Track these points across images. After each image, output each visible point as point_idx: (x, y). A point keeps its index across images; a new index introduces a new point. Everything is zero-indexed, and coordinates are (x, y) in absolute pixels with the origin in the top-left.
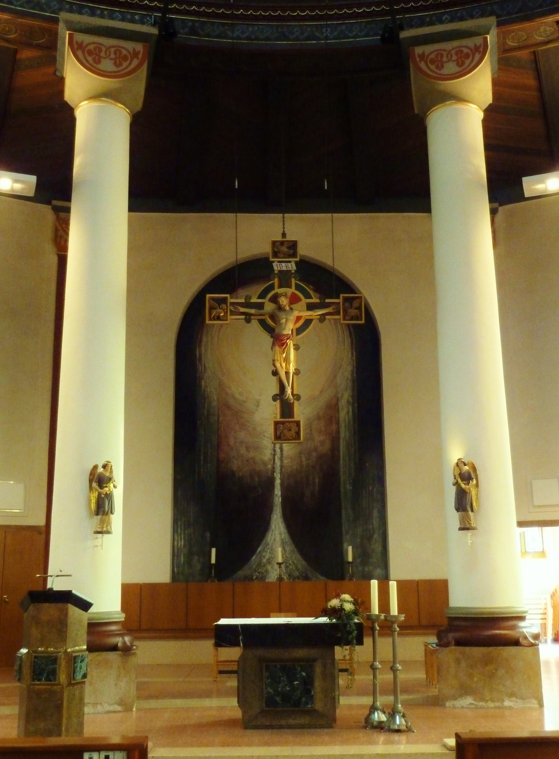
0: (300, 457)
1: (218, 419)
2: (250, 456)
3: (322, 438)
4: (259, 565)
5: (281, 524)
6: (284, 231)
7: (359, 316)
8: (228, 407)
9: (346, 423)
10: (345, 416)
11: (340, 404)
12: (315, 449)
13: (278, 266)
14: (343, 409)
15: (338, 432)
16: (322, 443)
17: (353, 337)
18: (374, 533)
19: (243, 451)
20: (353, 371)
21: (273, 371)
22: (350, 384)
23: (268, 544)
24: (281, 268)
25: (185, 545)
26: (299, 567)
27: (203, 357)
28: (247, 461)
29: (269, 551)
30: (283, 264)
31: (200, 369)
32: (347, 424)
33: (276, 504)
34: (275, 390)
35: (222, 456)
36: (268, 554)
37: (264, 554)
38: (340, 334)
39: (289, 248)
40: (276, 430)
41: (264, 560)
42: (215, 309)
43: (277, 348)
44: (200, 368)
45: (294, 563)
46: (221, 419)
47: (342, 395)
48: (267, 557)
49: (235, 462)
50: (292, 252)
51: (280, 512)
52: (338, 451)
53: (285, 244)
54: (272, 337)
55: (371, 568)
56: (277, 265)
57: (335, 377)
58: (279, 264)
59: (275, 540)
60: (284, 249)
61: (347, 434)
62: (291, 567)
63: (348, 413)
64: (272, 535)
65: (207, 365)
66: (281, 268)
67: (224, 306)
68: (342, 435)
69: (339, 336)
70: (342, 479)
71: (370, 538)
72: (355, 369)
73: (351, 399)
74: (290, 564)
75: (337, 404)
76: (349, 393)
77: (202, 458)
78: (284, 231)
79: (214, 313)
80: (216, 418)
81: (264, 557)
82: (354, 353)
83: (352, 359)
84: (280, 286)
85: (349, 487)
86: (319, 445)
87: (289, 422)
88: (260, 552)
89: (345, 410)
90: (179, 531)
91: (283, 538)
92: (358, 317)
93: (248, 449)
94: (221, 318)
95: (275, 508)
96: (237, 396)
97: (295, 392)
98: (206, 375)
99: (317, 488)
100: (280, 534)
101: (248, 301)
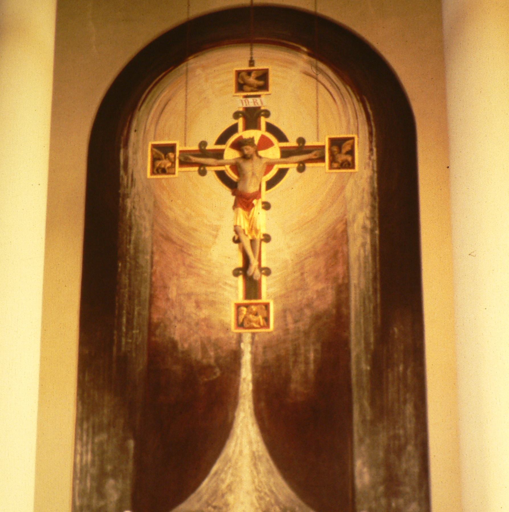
0: (285, 317)
1: (152, 258)
2: (202, 316)
3: (320, 286)
4: (215, 493)
5: (250, 427)
6: (252, 58)
7: (351, 163)
8: (168, 239)
9: (360, 264)
10: (359, 250)
11: (350, 231)
12: (309, 305)
13: (244, 102)
14: (355, 240)
15: (347, 276)
16: (321, 294)
17: (373, 124)
18: (406, 443)
19: (190, 307)
20: (371, 178)
21: (234, 238)
22: (367, 198)
23: (230, 460)
24: (247, 105)
25: (93, 461)
26: (281, 498)
27: (130, 162)
28: (197, 324)
29: (230, 471)
30: (250, 100)
31: (125, 182)
32: (362, 264)
33: (244, 393)
34: (239, 263)
35: (155, 318)
36: (229, 475)
37: (223, 476)
38: (352, 121)
39: (258, 78)
40: (238, 313)
41: (223, 487)
42: (159, 159)
43: (240, 210)
44: (125, 180)
45: (272, 492)
46: (156, 258)
47: (354, 216)
48: (228, 482)
49: (178, 326)
50: (261, 83)
51: (249, 408)
52: (348, 307)
53: (253, 75)
54: (234, 194)
55: (401, 501)
56: (242, 101)
57: (343, 188)
58: (245, 99)
59: (241, 452)
60: (252, 80)
61: (363, 280)
62: (268, 499)
63: (364, 245)
64: (236, 445)
65: (136, 176)
66: (247, 105)
67: (171, 155)
68: (354, 281)
69: (349, 123)
70: (354, 354)
71: (400, 451)
72: (376, 175)
73: (368, 224)
74: (266, 493)
75: (345, 231)
76: (366, 214)
77: (124, 320)
78: (252, 58)
79: (158, 163)
80: (148, 257)
81: (223, 481)
82: (375, 149)
83: (370, 158)
84: (247, 127)
85: (366, 367)
86: (315, 296)
87: (256, 304)
88: (216, 473)
89: (359, 241)
90: (85, 438)
91: (254, 449)
92: (349, 164)
93: (198, 305)
94: (167, 171)
95: (241, 401)
96: (182, 221)
97: (264, 264)
98: (134, 191)
99: (312, 367)
100: (250, 443)
101: (203, 148)
